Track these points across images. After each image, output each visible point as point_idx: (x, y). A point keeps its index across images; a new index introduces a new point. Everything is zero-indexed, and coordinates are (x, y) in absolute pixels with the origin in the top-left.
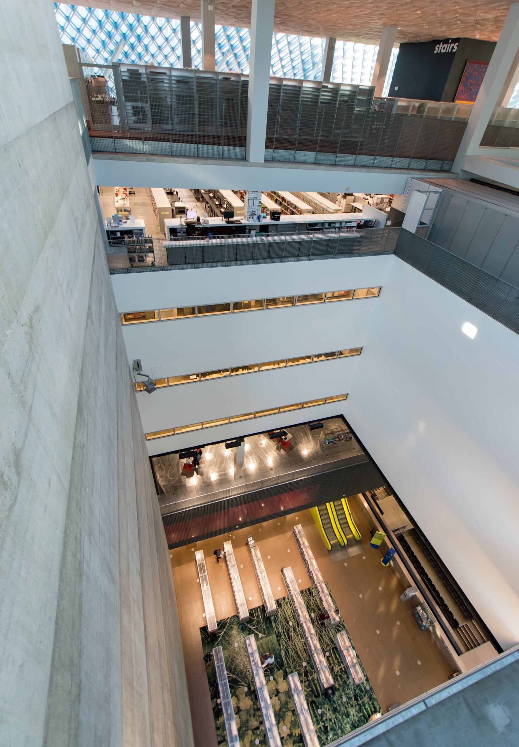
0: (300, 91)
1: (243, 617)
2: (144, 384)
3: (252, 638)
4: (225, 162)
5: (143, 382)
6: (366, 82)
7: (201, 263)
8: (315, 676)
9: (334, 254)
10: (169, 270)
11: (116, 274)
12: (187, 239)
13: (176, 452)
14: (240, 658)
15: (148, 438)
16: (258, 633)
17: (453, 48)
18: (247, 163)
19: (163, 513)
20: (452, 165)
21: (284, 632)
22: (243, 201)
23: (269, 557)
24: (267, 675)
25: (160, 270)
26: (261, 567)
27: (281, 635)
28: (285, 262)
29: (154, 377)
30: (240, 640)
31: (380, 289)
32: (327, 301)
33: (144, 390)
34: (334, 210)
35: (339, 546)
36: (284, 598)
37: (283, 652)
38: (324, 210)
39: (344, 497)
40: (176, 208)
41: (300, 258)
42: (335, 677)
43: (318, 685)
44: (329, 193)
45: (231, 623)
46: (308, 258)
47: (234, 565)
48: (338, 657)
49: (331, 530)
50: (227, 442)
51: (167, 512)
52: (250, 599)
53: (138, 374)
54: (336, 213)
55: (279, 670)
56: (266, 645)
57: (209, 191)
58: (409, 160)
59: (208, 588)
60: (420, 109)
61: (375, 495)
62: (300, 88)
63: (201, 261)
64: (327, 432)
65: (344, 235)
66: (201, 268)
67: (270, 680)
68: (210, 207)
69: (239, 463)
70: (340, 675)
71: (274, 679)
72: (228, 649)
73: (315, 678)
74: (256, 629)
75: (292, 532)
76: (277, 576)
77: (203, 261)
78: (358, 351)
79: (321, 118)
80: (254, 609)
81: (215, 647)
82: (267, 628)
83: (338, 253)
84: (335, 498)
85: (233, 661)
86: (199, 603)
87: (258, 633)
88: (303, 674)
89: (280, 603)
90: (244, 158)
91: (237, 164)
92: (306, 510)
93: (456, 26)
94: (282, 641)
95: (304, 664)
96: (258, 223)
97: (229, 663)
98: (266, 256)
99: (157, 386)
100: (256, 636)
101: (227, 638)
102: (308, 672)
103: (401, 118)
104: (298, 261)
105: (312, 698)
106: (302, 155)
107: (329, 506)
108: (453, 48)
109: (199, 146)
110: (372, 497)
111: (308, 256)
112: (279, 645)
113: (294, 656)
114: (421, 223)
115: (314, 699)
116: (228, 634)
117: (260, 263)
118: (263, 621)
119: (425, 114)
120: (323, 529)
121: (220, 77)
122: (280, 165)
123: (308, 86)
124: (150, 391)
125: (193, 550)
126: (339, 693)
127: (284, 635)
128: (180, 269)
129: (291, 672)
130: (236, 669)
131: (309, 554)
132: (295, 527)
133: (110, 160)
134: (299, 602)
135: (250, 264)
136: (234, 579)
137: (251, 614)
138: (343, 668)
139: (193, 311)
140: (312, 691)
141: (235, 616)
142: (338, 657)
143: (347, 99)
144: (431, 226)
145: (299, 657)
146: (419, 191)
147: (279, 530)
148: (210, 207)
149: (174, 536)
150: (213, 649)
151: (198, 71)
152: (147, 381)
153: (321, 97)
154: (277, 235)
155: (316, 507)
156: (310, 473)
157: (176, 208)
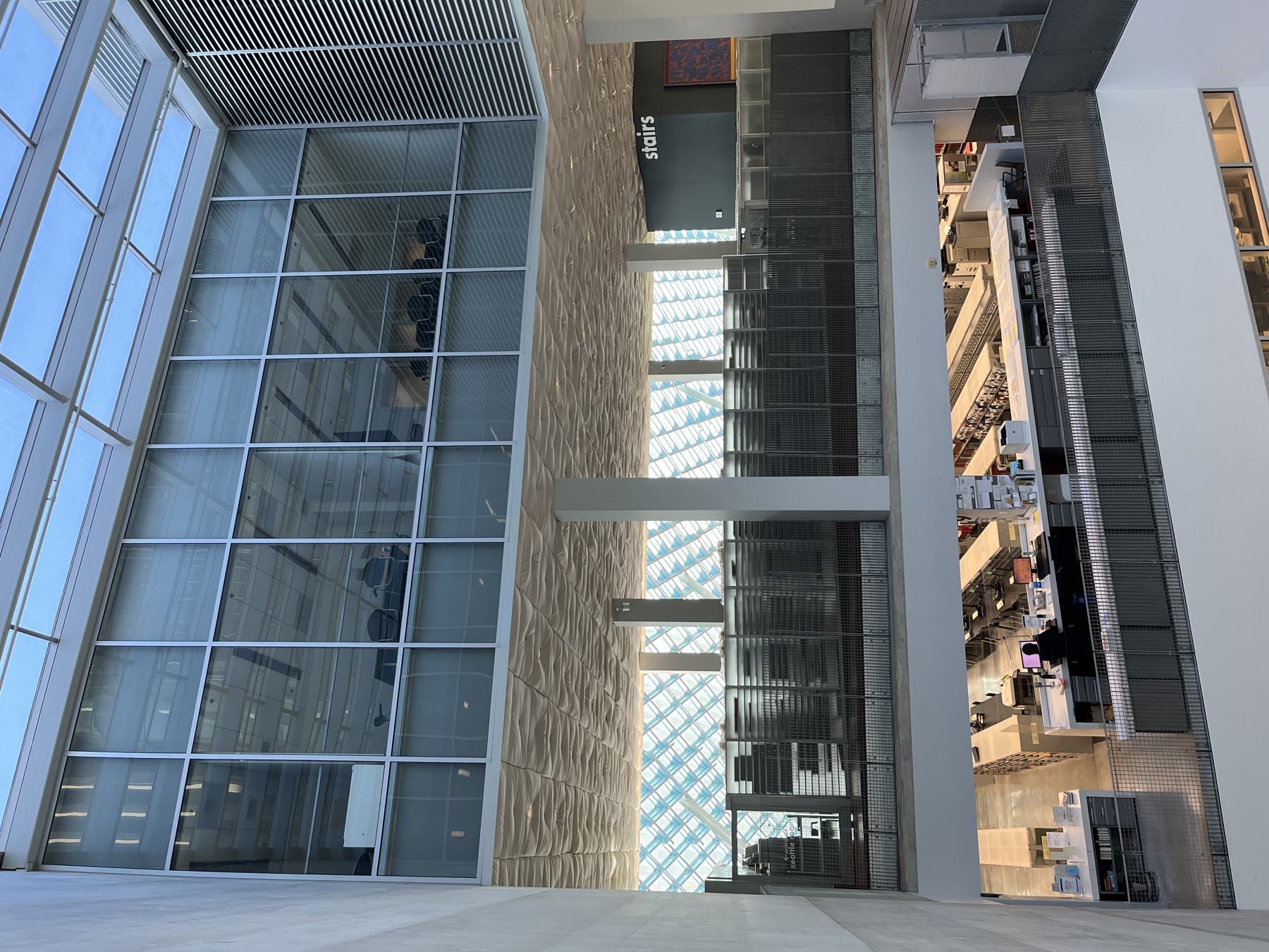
0: (743, 414)
4: (895, 569)
6: (714, 279)
7: (1174, 635)
9: (1108, 256)
10: (1206, 730)
11: (1232, 892)
17: (649, 125)
18: (892, 515)
20: (855, 31)
22: (985, 524)
25: (1210, 758)
28: (1146, 391)
31: (1207, 93)
38: (990, 312)
40: (1018, 704)
41: (1131, 348)
44: (945, 309)
54: (992, 279)
57: (967, 620)
58: (854, 137)
60: (753, 148)
62: (737, 413)
65: (1051, 242)
68: (1006, 614)
77: (1169, 627)
79: (770, 779)
83: (1107, 245)
90: (882, 521)
91: (898, 541)
93: (618, 133)
96: (1039, 476)
103: (771, 186)
104: (1139, 353)
106: (864, 391)
108: (649, 125)
109: (866, 631)
111: (1120, 327)
114: (1002, 47)
119: (763, 135)
121: (733, 583)
122: (890, 437)
123: (733, 400)
128: (1201, 699)
133: (915, 849)
143: (748, 312)
144: (1008, 19)
146: (923, 85)
148: (1006, 614)
151: (725, 635)
153: (750, 367)
154: (1068, 426)
157: (1018, 704)
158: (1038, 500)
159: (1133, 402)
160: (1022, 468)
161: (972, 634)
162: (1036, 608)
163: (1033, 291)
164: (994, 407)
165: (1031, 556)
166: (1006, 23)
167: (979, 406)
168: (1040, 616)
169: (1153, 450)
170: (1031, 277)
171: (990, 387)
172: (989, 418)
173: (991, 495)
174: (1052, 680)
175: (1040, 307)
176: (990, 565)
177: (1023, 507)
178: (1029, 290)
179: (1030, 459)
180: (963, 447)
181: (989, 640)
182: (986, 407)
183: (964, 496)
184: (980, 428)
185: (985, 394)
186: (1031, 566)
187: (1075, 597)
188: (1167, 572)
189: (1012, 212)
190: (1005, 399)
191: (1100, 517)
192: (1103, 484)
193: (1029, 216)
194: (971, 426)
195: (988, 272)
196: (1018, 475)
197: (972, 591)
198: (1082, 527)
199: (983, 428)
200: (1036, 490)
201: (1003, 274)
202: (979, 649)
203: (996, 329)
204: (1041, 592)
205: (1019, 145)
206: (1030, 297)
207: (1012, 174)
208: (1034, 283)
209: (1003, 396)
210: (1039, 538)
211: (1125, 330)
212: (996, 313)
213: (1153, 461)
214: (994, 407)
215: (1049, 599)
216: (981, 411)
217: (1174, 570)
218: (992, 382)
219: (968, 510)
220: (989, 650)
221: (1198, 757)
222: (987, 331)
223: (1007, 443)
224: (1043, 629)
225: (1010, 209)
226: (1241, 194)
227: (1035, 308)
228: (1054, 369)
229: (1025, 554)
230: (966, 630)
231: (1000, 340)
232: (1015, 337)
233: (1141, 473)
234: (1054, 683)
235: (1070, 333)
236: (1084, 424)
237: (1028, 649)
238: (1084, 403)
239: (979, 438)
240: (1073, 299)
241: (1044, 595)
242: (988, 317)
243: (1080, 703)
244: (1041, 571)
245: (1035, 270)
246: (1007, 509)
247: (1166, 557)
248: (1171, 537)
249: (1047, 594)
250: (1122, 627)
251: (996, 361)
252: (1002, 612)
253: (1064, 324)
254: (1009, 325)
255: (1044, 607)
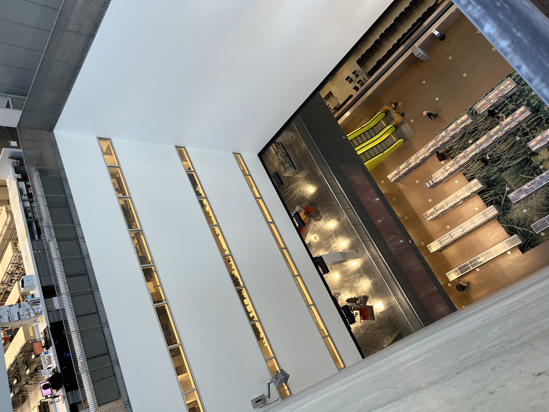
1: (496, 211)
2: (279, 388)
3: (511, 196)
5: (278, 388)
8: (524, 125)
9: (66, 198)
12: (82, 386)
13: (349, 329)
14: (535, 203)
15: (343, 366)
16: (506, 191)
19: (420, 326)
21: (496, 166)
23: (430, 200)
24: (541, 171)
26: (444, 205)
27: (499, 169)
29: (268, 377)
30: (519, 208)
31: (100, 139)
32: (128, 195)
33: (286, 385)
34: (8, 215)
35: (398, 132)
36: (465, 174)
37: (515, 162)
38: (11, 227)
39: (346, 137)
41: (80, 236)
42: (519, 106)
43: (531, 121)
45: (507, 223)
46: (78, 226)
47: (450, 234)
48: (500, 108)
49: (383, 144)
50: (322, 272)
51: (418, 323)
52: (477, 209)
53: (269, 398)
54: (11, 212)
55: (532, 161)
56: (514, 181)
57: (12, 387)
59: (482, 256)
61: (335, 108)
63: (107, 356)
64: (283, 170)
65: (39, 190)
66: (116, 354)
67: (544, 168)
69: (344, 257)
70: (515, 102)
71: (541, 164)
72: (531, 218)
73: (526, 125)
74: (503, 194)
75: (398, 184)
76: (447, 187)
77: (108, 353)
78: (181, 152)
80: (485, 202)
81: (534, 231)
82: (498, 184)
83: (65, 194)
84: (350, 147)
85: (540, 209)
86: (500, 261)
87: (506, 191)
88: (526, 137)
89: (470, 178)
92: (372, 174)
94: (506, 165)
95: (518, 138)
97: (543, 213)
98: (86, 277)
99: (278, 369)
100: (509, 193)
101: (522, 222)
102: (523, 133)
104: (83, 238)
105: (544, 124)
107: (360, 150)
110: (338, 110)
111: (74, 227)
112: (509, 167)
113: (514, 150)
115: (544, 121)
116: (518, 222)
117: (96, 282)
118: (493, 189)
120: (385, 152)
124: (285, 376)
125: (449, 285)
126: (531, 99)
127: (498, 165)
128: (123, 381)
129: (529, 149)
130: (546, 205)
131: (413, 160)
132: (392, 181)
134: (462, 158)
135: (100, 295)
136: (463, 231)
137: (491, 203)
138: (508, 100)
139: (175, 353)
140: (538, 125)
141: (499, 220)
142: (500, 108)
144: (10, 95)
145: (513, 145)
147: (401, 198)
149: (442, 308)
150: (537, 233)
152: (275, 383)
154: (55, 274)
155: (365, 164)
156: (331, 177)
158: (43, 311)
159: (83, 259)
160: (34, 297)
161: (14, 393)
162: (46, 365)
163: (33, 216)
164: (17, 274)
165: (41, 340)
166: (10, 97)
167: (9, 274)
168: (49, 368)
169: (93, 278)
170: (31, 209)
171: (14, 264)
172: (14, 279)
173: (18, 313)
174: (57, 398)
175: (37, 222)
176: (20, 353)
177: (35, 316)
178: (30, 215)
179: (37, 293)
180: (2, 297)
181: (24, 394)
182: (12, 274)
183: (4, 316)
184: (10, 286)
185: (11, 267)
186: (42, 345)
187: (65, 354)
188: (94, 293)
189: (18, 180)
190: (22, 269)
191: (73, 311)
192: (73, 296)
193: (27, 182)
194: (5, 285)
195: (8, 209)
196: (31, 301)
197: (12, 368)
198: (66, 320)
199: (12, 285)
200: (42, 306)
201: (16, 208)
202: (19, 401)
203: (15, 236)
204: (48, 356)
205: (20, 150)
206: (31, 218)
207: (17, 163)
208: (33, 212)
209: (21, 267)
210: (45, 330)
211: (76, 228)
212: (14, 228)
213: (94, 282)
214: (17, 274)
215: (52, 358)
216: (10, 276)
217: (107, 328)
218: (15, 261)
219: (7, 323)
220: (24, 398)
221: (125, 408)
222: (10, 237)
223: (25, 286)
224: (51, 374)
225: (17, 178)
226: (116, 179)
227: (34, 223)
228: (46, 249)
229: (38, 339)
230: (11, 392)
231: (18, 240)
232: (25, 236)
233: (89, 288)
234: (59, 399)
235: (52, 230)
236: (62, 270)
237: (45, 387)
238: (64, 272)
239: (10, 291)
240: (51, 216)
241: (50, 357)
242: (10, 231)
243: (72, 404)
244: (47, 346)
245: (32, 206)
246: (28, 319)
247: (103, 323)
248: (104, 313)
249: (51, 356)
250: (87, 359)
251: (16, 250)
252: (29, 375)
253: (48, 226)
254: (21, 231)
255: (51, 363)
